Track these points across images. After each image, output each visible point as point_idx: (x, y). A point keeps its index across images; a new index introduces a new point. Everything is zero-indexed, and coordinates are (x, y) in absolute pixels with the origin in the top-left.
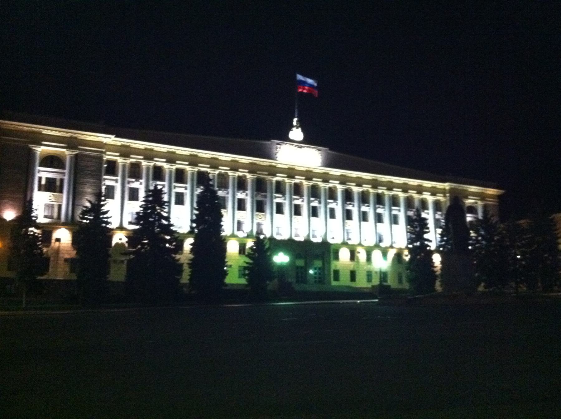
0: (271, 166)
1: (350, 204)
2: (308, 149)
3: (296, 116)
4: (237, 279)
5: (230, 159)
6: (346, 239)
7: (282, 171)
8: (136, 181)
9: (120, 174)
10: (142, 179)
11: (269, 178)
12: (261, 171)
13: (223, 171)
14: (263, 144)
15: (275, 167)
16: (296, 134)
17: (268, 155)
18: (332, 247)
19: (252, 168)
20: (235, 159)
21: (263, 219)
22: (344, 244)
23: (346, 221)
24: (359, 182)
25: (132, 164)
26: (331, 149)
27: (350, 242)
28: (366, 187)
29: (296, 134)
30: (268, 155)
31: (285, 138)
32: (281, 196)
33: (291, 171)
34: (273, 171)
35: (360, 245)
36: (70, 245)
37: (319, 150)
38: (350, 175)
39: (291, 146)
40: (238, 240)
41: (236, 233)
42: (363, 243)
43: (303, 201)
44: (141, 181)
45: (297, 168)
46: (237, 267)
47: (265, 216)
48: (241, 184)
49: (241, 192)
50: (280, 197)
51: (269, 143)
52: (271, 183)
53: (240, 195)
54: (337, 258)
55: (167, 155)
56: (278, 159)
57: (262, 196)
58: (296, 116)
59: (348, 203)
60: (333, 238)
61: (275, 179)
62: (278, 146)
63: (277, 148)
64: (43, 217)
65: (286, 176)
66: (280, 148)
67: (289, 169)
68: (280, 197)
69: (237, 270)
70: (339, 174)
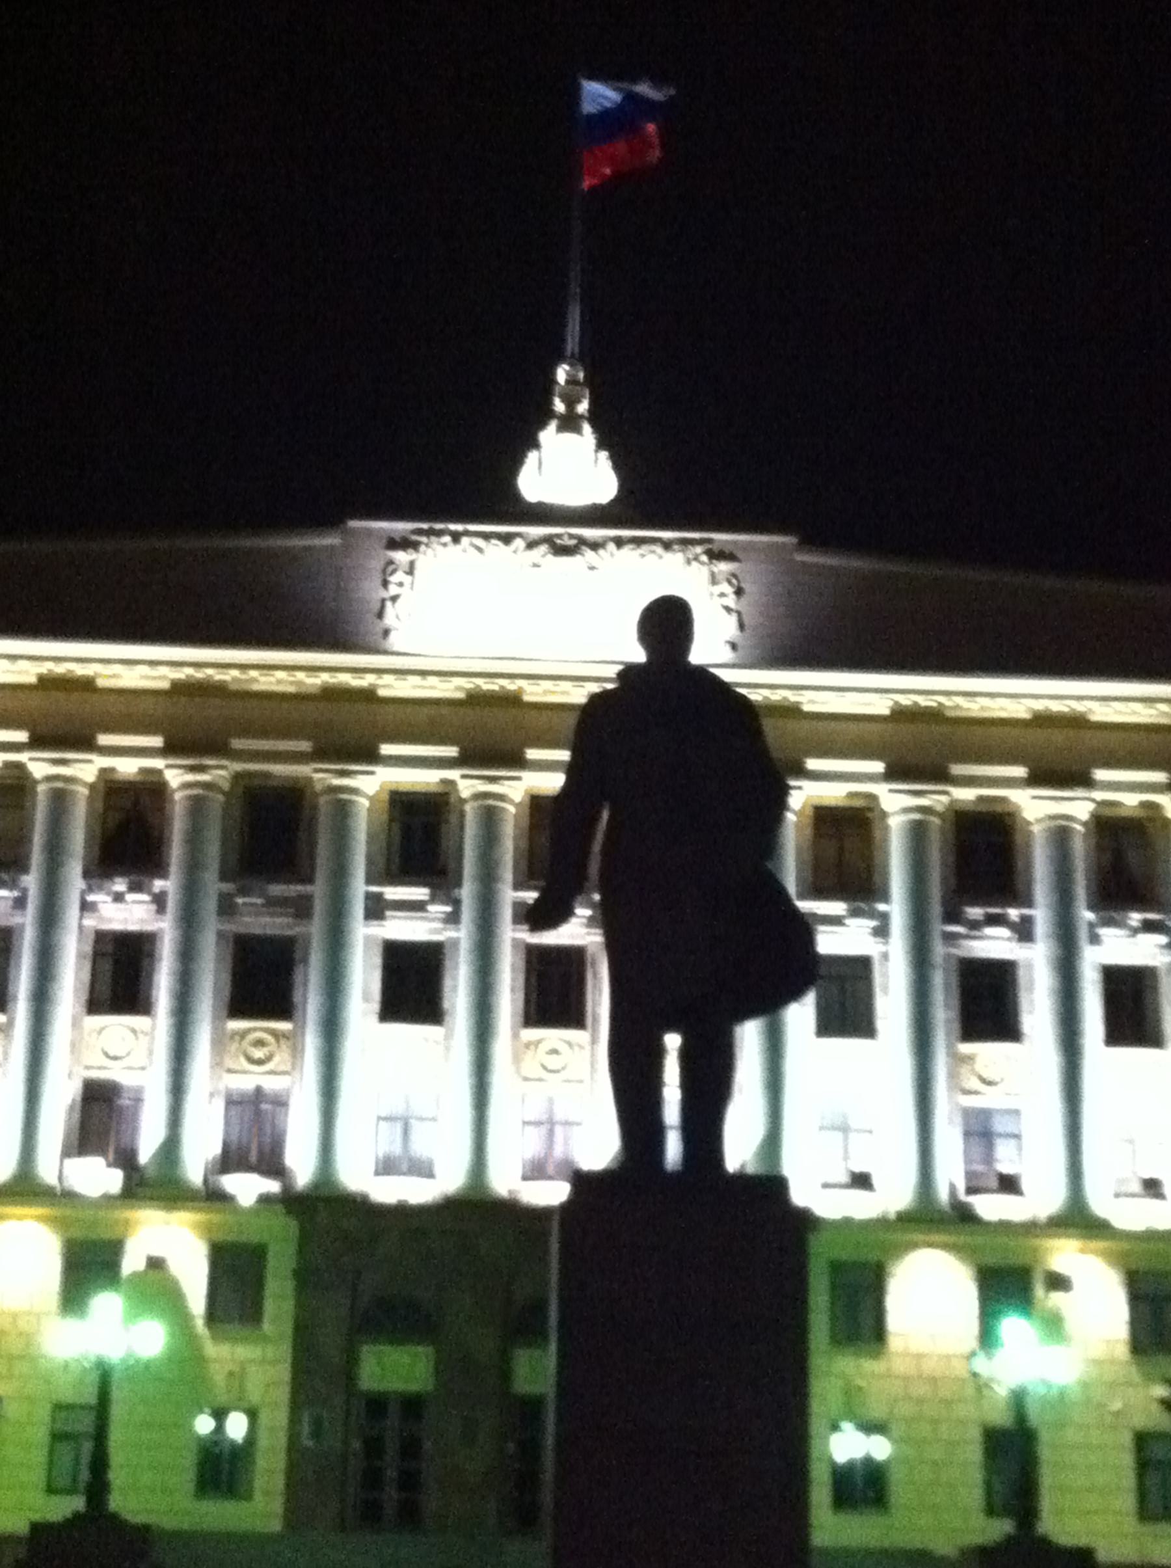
0: (331, 694)
1: (995, 920)
2: (627, 552)
3: (572, 343)
4: (1130, 1523)
5: (881, 706)
6: (950, 1173)
7: (422, 721)
8: (855, 913)
9: (176, 852)
10: (164, 876)
11: (321, 776)
12: (264, 734)
13: (1131, 800)
14: (294, 557)
15: (368, 696)
16: (567, 465)
17: (329, 623)
18: (820, 1255)
19: (194, 722)
20: (60, 669)
21: (281, 1059)
22: (937, 1219)
23: (966, 1048)
24: (1061, 755)
25: (111, 789)
26: (813, 537)
27: (991, 1207)
28: (129, 758)
29: (567, 465)
30: (329, 623)
31: (482, 494)
32: (419, 893)
33: (1058, 737)
34: (352, 728)
35: (1077, 1219)
36: (1122, 1350)
37: (716, 555)
38: (974, 708)
39: (496, 547)
40: (57, 1223)
41: (47, 1169)
42: (1100, 1204)
43: (453, 919)
44: (158, 884)
45: (534, 693)
46: (43, 1413)
47: (294, 1041)
48: (128, 837)
49: (120, 885)
50: (416, 906)
51: (331, 540)
52: (490, 817)
53: (126, 910)
54: (864, 1323)
55: (36, 701)
56: (395, 641)
57: (275, 904)
58: (572, 343)
59: (975, 912)
60: (1152, 1187)
61: (370, 784)
62: (401, 557)
63: (389, 566)
64: (820, 1186)
65: (451, 751)
66: (410, 571)
67: (475, 699)
68: (416, 906)
69: (40, 1434)
70: (159, 679)
